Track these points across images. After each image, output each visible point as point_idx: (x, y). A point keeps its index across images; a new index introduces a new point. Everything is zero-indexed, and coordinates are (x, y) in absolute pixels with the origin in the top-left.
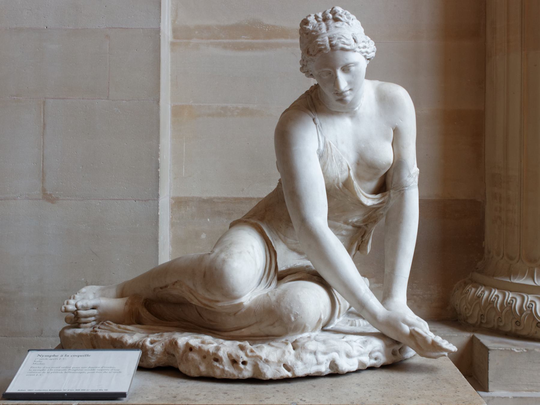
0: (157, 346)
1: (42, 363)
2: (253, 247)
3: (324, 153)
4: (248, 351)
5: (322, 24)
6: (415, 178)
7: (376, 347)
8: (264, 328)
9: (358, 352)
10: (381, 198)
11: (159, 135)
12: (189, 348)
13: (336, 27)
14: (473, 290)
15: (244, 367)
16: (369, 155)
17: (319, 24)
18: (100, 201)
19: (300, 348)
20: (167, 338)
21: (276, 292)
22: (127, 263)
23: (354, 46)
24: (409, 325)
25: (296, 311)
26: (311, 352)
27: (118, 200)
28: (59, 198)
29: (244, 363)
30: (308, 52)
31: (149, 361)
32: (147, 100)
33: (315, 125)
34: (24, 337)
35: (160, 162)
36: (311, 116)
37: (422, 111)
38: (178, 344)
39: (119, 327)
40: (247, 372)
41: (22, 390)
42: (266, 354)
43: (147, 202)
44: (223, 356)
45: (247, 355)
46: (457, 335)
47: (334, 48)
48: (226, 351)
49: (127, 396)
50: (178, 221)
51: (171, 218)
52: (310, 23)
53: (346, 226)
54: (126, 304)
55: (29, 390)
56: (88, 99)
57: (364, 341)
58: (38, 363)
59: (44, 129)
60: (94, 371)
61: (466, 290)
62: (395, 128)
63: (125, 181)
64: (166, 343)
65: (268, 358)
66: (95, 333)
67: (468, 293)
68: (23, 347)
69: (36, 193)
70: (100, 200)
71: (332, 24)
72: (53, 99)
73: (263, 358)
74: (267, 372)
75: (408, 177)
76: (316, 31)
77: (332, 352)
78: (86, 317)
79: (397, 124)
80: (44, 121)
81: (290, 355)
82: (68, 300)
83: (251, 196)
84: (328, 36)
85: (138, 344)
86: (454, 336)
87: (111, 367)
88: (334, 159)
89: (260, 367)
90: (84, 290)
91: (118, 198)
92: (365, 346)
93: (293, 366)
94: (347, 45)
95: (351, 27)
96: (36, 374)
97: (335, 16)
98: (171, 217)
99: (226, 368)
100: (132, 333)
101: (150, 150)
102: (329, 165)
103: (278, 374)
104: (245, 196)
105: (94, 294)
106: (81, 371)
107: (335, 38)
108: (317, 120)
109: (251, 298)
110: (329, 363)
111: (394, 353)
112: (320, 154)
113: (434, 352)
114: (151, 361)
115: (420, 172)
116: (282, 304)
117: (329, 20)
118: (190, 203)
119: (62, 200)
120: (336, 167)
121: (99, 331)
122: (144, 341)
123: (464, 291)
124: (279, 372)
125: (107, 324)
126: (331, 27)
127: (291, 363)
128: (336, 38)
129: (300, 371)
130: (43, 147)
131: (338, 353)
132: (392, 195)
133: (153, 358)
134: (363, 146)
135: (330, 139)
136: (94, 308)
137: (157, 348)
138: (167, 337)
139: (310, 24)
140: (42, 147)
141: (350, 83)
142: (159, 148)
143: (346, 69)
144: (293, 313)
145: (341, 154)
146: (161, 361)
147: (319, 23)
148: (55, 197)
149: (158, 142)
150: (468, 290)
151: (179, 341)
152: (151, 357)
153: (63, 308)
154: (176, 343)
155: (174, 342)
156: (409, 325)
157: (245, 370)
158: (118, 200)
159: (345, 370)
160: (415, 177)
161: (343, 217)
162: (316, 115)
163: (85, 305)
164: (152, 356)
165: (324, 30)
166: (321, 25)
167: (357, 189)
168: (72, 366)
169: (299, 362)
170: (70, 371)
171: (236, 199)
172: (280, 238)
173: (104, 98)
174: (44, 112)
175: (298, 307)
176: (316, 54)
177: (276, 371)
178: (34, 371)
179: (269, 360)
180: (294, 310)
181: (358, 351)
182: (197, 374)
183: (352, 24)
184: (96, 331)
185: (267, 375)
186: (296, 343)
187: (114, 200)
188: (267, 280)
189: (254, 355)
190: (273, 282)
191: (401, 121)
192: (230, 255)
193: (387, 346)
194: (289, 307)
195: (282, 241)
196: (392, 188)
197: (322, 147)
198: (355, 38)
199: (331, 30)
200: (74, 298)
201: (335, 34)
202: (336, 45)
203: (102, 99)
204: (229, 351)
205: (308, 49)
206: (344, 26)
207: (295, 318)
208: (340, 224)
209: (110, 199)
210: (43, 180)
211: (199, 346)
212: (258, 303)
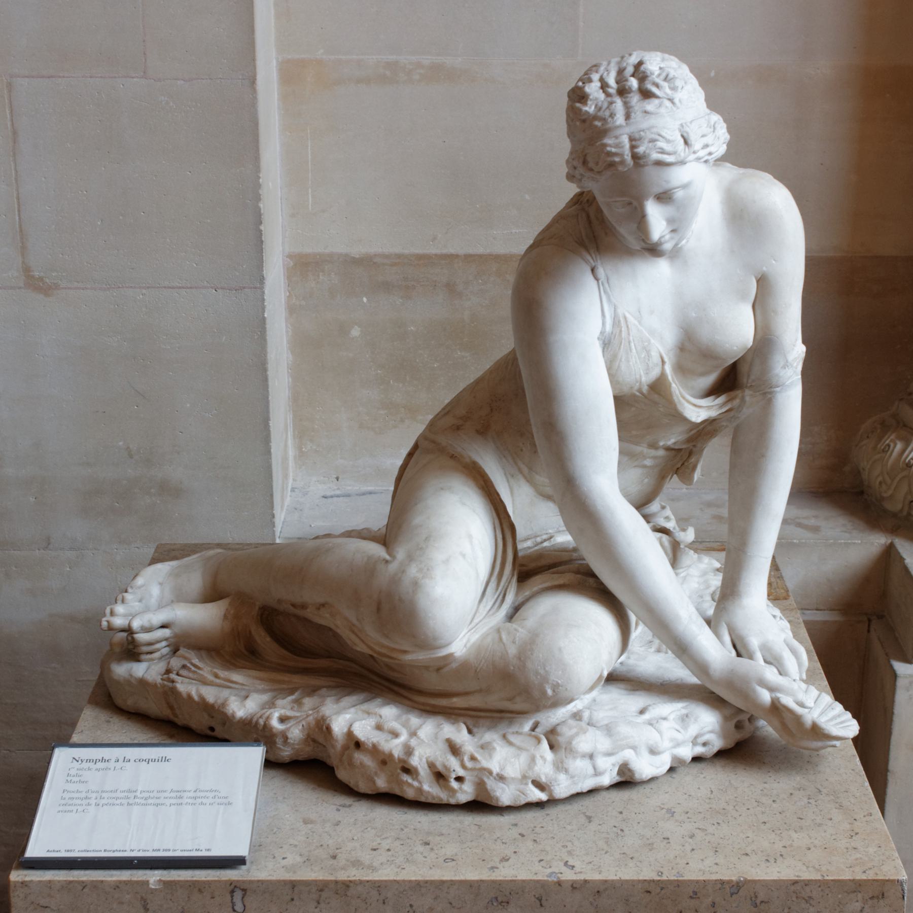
0: (292, 729)
1: (82, 779)
2: (470, 537)
3: (613, 338)
4: (466, 759)
5: (615, 102)
6: (796, 368)
7: (704, 728)
8: (494, 701)
9: (672, 741)
10: (724, 404)
11: (259, 154)
12: (353, 742)
13: (646, 112)
14: (899, 446)
15: (459, 786)
16: (705, 335)
17: (609, 102)
18: (144, 291)
19: (564, 750)
20: (310, 712)
21: (518, 634)
22: (206, 413)
23: (682, 154)
24: (771, 689)
25: (555, 679)
26: (584, 756)
27: (180, 288)
28: (59, 286)
29: (459, 779)
30: (585, 162)
31: (280, 754)
32: (229, 79)
33: (596, 282)
34: (14, 550)
35: (262, 212)
36: (587, 262)
37: (818, 69)
38: (333, 733)
39: (216, 676)
40: (466, 792)
41: (54, 851)
42: (500, 765)
43: (240, 291)
44: (419, 766)
45: (464, 767)
46: (860, 542)
47: (641, 162)
48: (425, 756)
49: (248, 863)
50: (303, 303)
51: (288, 297)
52: (591, 100)
53: (653, 452)
54: (225, 617)
55: (68, 851)
56: (101, 77)
57: (684, 715)
58: (75, 779)
59: (15, 143)
60: (180, 801)
61: (885, 445)
62: (760, 276)
63: (193, 250)
64: (309, 724)
65: (503, 773)
66: (170, 684)
67: (887, 451)
68: (14, 569)
69: (11, 276)
70: (144, 288)
71: (638, 104)
72: (27, 77)
73: (495, 773)
74: (503, 796)
75: (782, 368)
76: (604, 120)
77: (623, 750)
78: (150, 644)
79: (764, 269)
80: (13, 125)
81: (545, 763)
82: (112, 606)
83: (452, 251)
84: (628, 134)
85: (257, 723)
86: (854, 543)
87: (211, 791)
88: (633, 347)
89: (489, 787)
90: (140, 581)
91: (181, 285)
92: (685, 728)
93: (551, 783)
94: (669, 154)
95: (678, 108)
96: (75, 808)
97: (644, 84)
98: (288, 294)
99: (426, 787)
100: (242, 689)
101: (241, 186)
102: (623, 360)
103: (521, 799)
104: (438, 252)
105: (161, 584)
106: (158, 801)
107: (644, 139)
108: (601, 272)
109: (468, 641)
110: (616, 769)
111: (739, 726)
112: (605, 338)
113: (815, 740)
114: (282, 754)
115: (808, 352)
116: (529, 665)
117: (632, 95)
118: (326, 267)
119: (66, 288)
120: (636, 362)
121: (180, 682)
122: (268, 718)
123: (879, 446)
124: (524, 794)
125: (193, 668)
126: (635, 113)
127: (546, 777)
128: (646, 141)
129: (563, 789)
130: (16, 180)
131: (634, 750)
132: (747, 399)
133: (286, 749)
134: (694, 315)
135: (626, 308)
136: (163, 626)
137: (292, 733)
138: (310, 710)
139: (589, 102)
140: (14, 181)
141: (670, 221)
142: (259, 182)
143: (664, 197)
144: (550, 682)
145: (647, 335)
146: (302, 753)
147: (609, 99)
148: (50, 284)
149: (258, 169)
150: (889, 446)
151: (334, 725)
152: (282, 747)
153: (104, 624)
154: (329, 729)
155: (324, 727)
156: (771, 689)
157: (460, 792)
158: (180, 288)
159: (646, 778)
160: (797, 365)
161: (648, 437)
162: (598, 257)
163: (147, 624)
164: (284, 746)
165: (620, 119)
166: (614, 105)
167: (678, 397)
168: (140, 789)
169: (562, 774)
170: (137, 800)
171: (420, 257)
172: (521, 471)
173: (137, 75)
174: (11, 107)
175: (560, 672)
176: (602, 171)
177: (518, 793)
178: (70, 802)
179: (506, 775)
180: (553, 678)
181: (672, 740)
182: (372, 791)
183: (680, 101)
184: (173, 681)
185: (501, 800)
186: (556, 737)
187: (173, 288)
188: (497, 589)
189: (478, 766)
190: (509, 593)
191: (774, 262)
192: (428, 569)
193: (726, 719)
194: (542, 672)
195: (525, 478)
196: (749, 385)
197: (608, 328)
198: (685, 135)
199: (635, 118)
200: (123, 601)
201: (643, 131)
202: (645, 156)
203: (133, 78)
204: (429, 757)
205: (586, 155)
206: (662, 110)
207: (554, 691)
208: (642, 449)
209: (165, 287)
210: (23, 249)
211: (372, 742)
212: (482, 655)
